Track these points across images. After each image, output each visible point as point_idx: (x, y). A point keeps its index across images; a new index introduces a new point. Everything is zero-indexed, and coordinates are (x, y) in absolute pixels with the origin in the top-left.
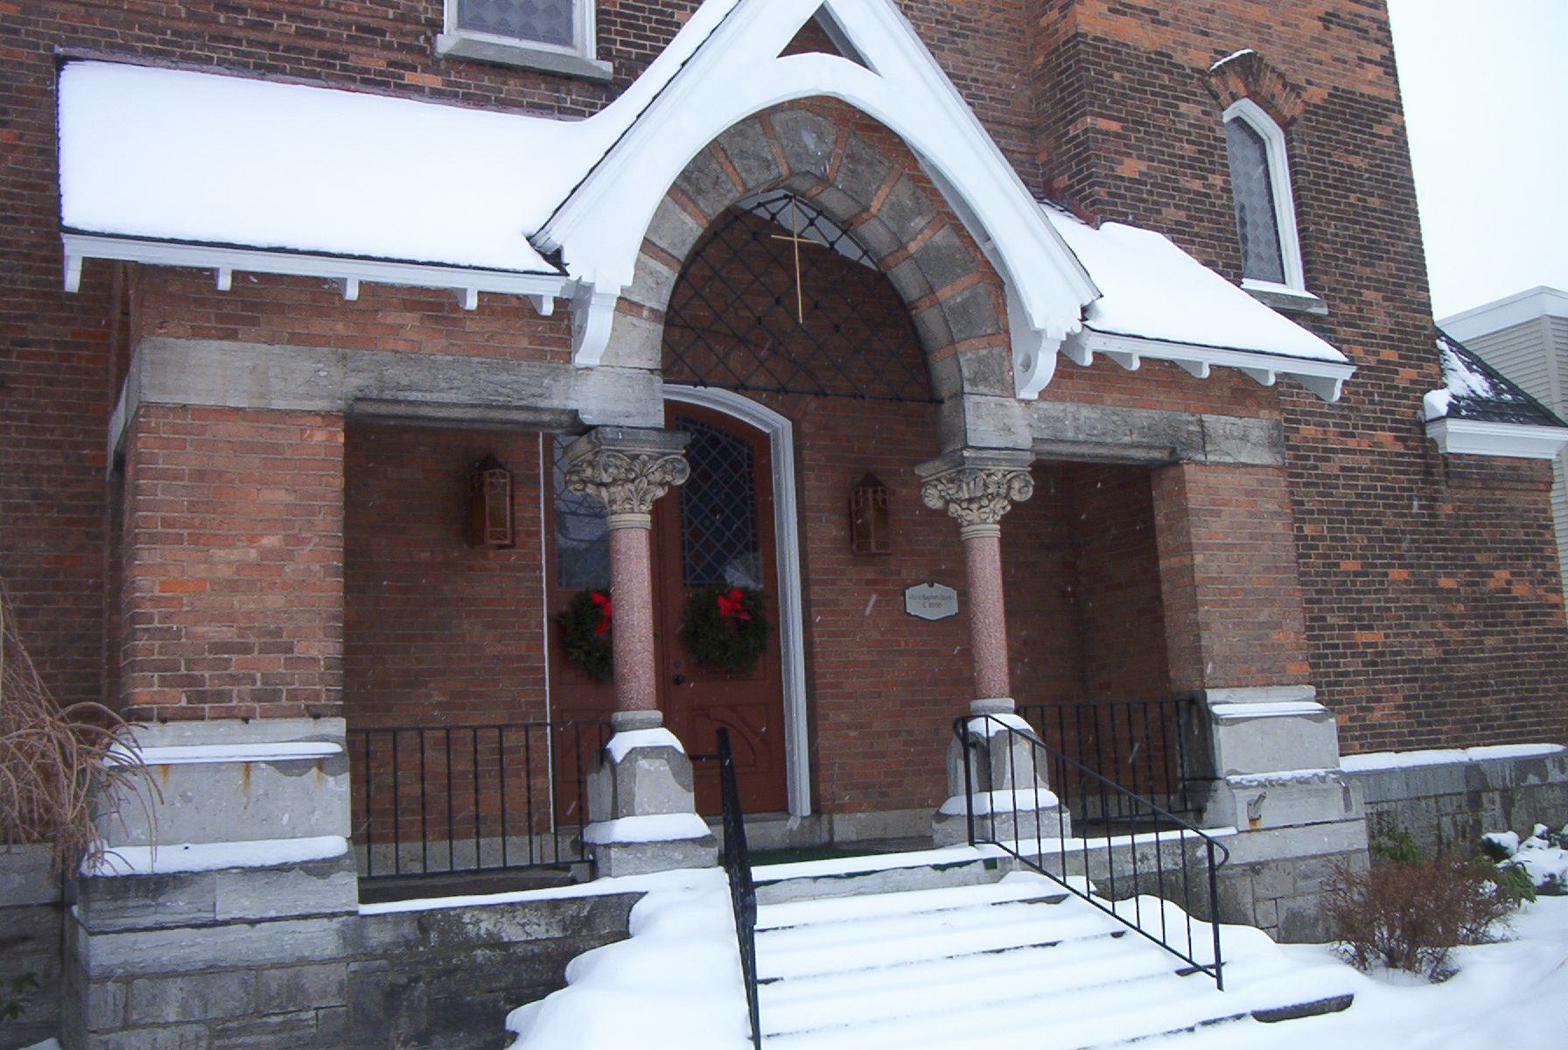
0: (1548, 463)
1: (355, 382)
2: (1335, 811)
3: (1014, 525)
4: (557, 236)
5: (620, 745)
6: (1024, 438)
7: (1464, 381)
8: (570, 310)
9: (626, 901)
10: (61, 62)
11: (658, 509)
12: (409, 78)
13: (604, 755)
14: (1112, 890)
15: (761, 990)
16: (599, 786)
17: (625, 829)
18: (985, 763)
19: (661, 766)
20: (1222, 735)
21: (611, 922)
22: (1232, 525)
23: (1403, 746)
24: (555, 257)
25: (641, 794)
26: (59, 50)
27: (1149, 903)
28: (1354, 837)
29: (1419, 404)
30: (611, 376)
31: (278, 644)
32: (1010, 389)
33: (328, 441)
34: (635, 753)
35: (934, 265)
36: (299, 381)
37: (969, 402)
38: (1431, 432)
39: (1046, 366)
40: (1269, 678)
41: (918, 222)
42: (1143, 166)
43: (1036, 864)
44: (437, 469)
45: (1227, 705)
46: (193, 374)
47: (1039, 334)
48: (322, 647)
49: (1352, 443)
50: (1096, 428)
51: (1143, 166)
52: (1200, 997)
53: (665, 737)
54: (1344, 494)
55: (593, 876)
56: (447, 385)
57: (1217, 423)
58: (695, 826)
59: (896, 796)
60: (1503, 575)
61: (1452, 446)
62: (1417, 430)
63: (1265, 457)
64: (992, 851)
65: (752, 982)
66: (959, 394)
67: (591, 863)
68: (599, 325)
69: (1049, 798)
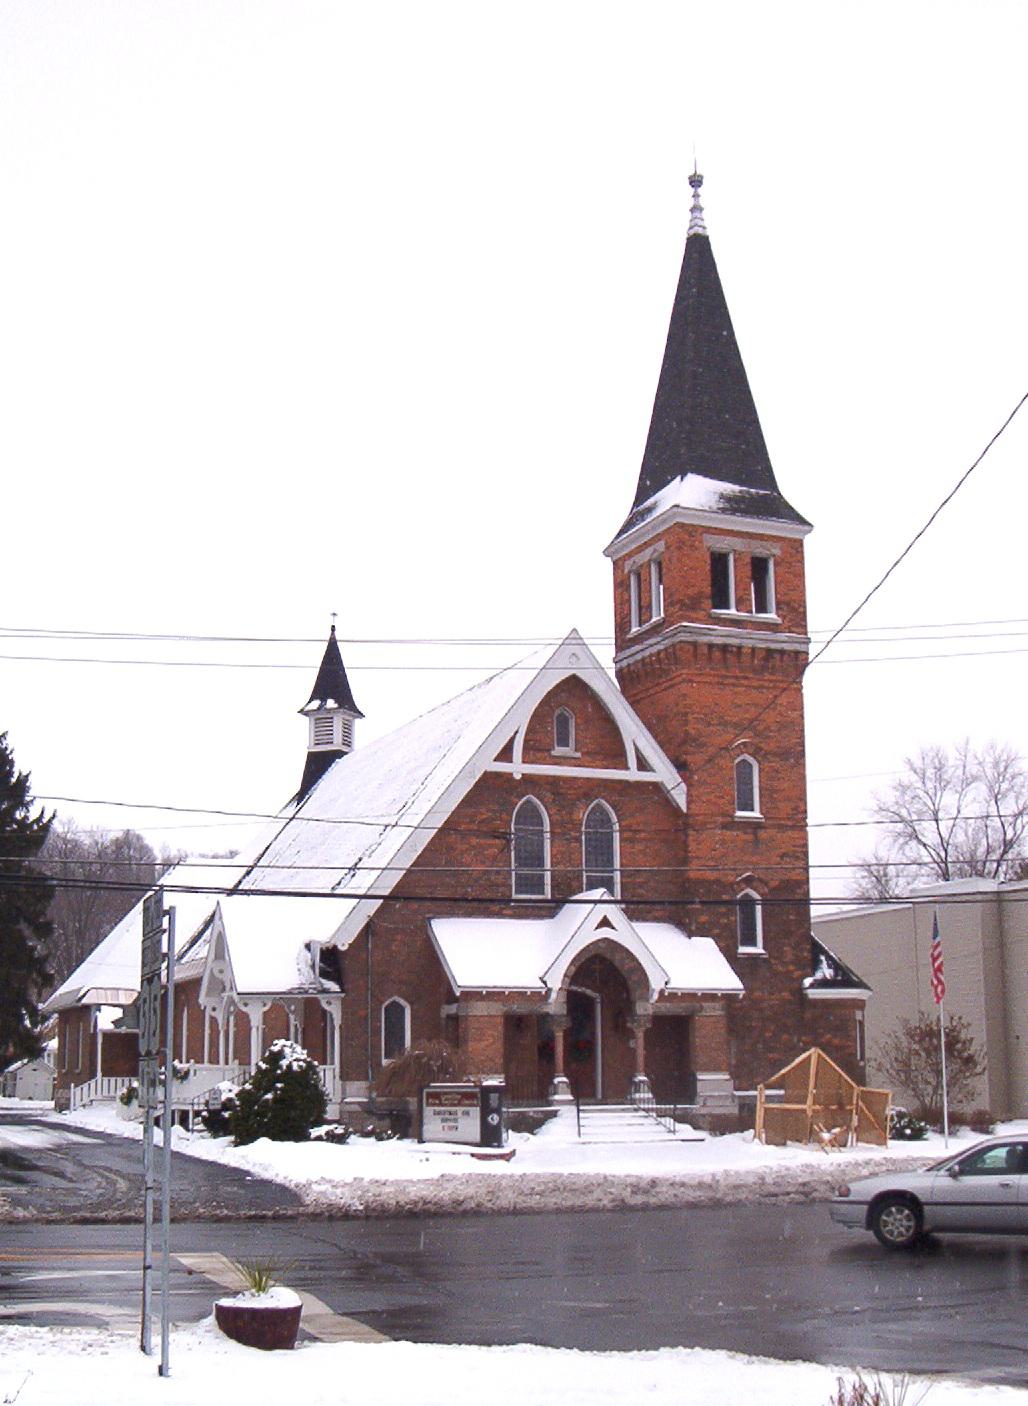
0: (863, 1001)
1: (506, 1009)
2: (728, 1102)
3: (647, 1033)
4: (545, 979)
5: (556, 1081)
6: (651, 1012)
7: (825, 971)
8: (549, 990)
9: (556, 1111)
10: (429, 919)
11: (565, 1031)
12: (505, 912)
13: (552, 1083)
14: (661, 1114)
15: (582, 1128)
16: (551, 1089)
17: (557, 1097)
18: (637, 1087)
19: (565, 1085)
20: (699, 1084)
21: (554, 1114)
22: (708, 1031)
23: (452, 1082)
24: (545, 983)
25: (560, 1090)
26: (427, 916)
27: (668, 1119)
28: (735, 1111)
29: (801, 983)
30: (556, 1005)
31: (492, 1060)
32: (648, 1000)
33: (500, 1020)
34: (559, 1082)
35: (631, 971)
36: (496, 1009)
37: (637, 1005)
38: (805, 992)
39: (656, 996)
40: (717, 1069)
41: (627, 961)
42: (707, 918)
43: (644, 1110)
44: (520, 1018)
45: (700, 1077)
46: (479, 1009)
47: (654, 990)
48: (500, 1061)
49: (773, 997)
50: (667, 1008)
51: (707, 918)
52: (671, 1136)
53: (565, 1079)
54: (768, 1013)
55: (549, 1106)
56: (518, 1008)
57: (705, 1005)
58: (571, 1097)
59: (618, 1093)
60: (829, 1036)
61: (810, 996)
62: (801, 989)
63: (722, 1013)
64: (635, 1106)
65: (579, 1126)
66: (635, 1003)
67: (550, 1104)
68: (554, 995)
69: (650, 1095)
